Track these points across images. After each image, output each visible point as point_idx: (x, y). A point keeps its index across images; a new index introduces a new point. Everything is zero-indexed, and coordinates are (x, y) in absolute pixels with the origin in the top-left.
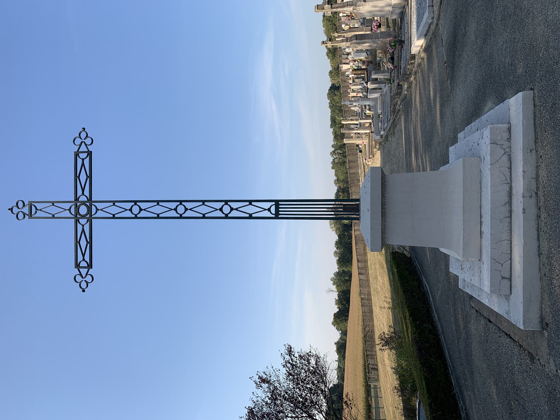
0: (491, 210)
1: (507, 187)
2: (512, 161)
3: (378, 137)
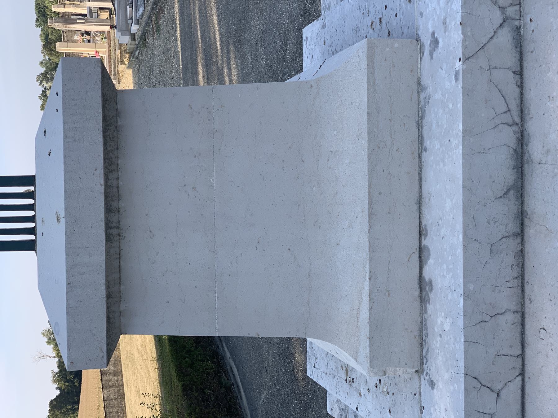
0: (465, 212)
1: (508, 136)
2: (528, 47)
3: (126, 39)
